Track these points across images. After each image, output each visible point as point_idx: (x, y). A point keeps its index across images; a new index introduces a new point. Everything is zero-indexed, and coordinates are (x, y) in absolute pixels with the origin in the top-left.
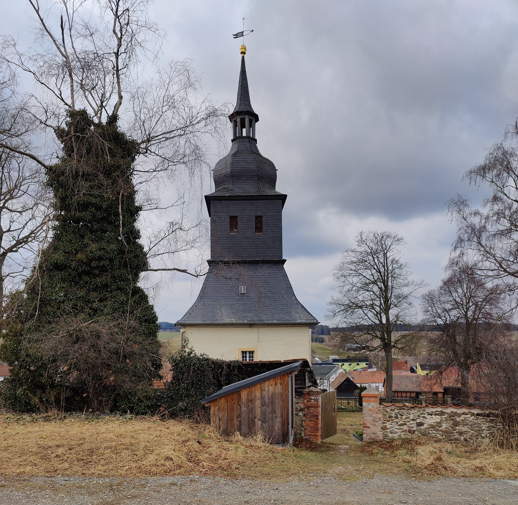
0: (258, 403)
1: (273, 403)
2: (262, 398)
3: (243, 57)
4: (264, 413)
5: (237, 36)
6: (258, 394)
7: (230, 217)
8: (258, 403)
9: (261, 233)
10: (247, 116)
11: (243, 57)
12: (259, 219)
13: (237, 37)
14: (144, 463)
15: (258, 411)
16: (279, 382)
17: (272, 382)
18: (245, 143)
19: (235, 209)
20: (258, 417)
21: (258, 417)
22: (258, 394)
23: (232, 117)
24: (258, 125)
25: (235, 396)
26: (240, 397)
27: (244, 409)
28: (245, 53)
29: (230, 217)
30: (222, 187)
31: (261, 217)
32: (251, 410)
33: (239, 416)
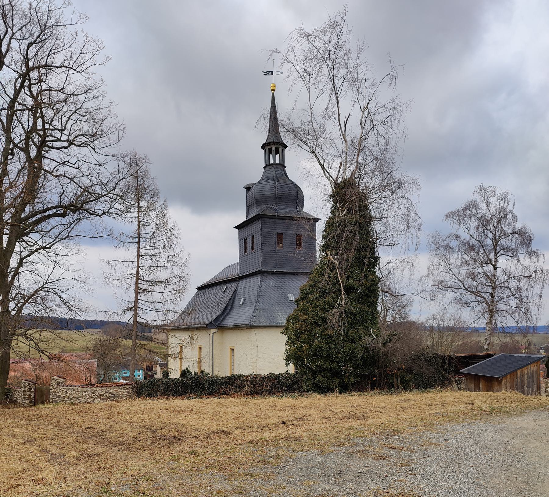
0: (526, 377)
1: (533, 376)
2: (528, 373)
3: (273, 94)
4: (528, 382)
5: (266, 73)
6: (526, 372)
7: (277, 233)
8: (526, 377)
9: (300, 249)
10: (273, 146)
11: (273, 94)
12: (280, 235)
13: (266, 75)
14: (116, 425)
15: (526, 381)
16: (535, 364)
17: (532, 365)
18: (276, 171)
19: (248, 231)
20: (526, 384)
21: (526, 384)
22: (526, 372)
23: (263, 147)
24: (286, 151)
25: (515, 373)
26: (517, 373)
27: (519, 380)
28: (274, 90)
29: (277, 233)
30: (265, 206)
31: (301, 236)
32: (523, 381)
33: (517, 385)
